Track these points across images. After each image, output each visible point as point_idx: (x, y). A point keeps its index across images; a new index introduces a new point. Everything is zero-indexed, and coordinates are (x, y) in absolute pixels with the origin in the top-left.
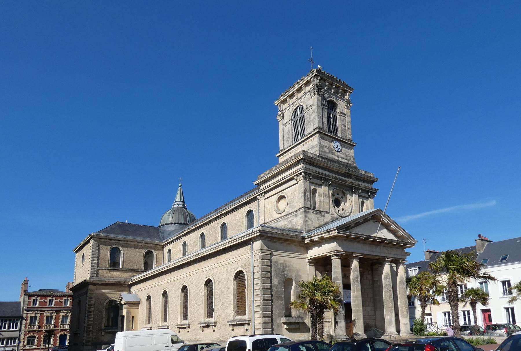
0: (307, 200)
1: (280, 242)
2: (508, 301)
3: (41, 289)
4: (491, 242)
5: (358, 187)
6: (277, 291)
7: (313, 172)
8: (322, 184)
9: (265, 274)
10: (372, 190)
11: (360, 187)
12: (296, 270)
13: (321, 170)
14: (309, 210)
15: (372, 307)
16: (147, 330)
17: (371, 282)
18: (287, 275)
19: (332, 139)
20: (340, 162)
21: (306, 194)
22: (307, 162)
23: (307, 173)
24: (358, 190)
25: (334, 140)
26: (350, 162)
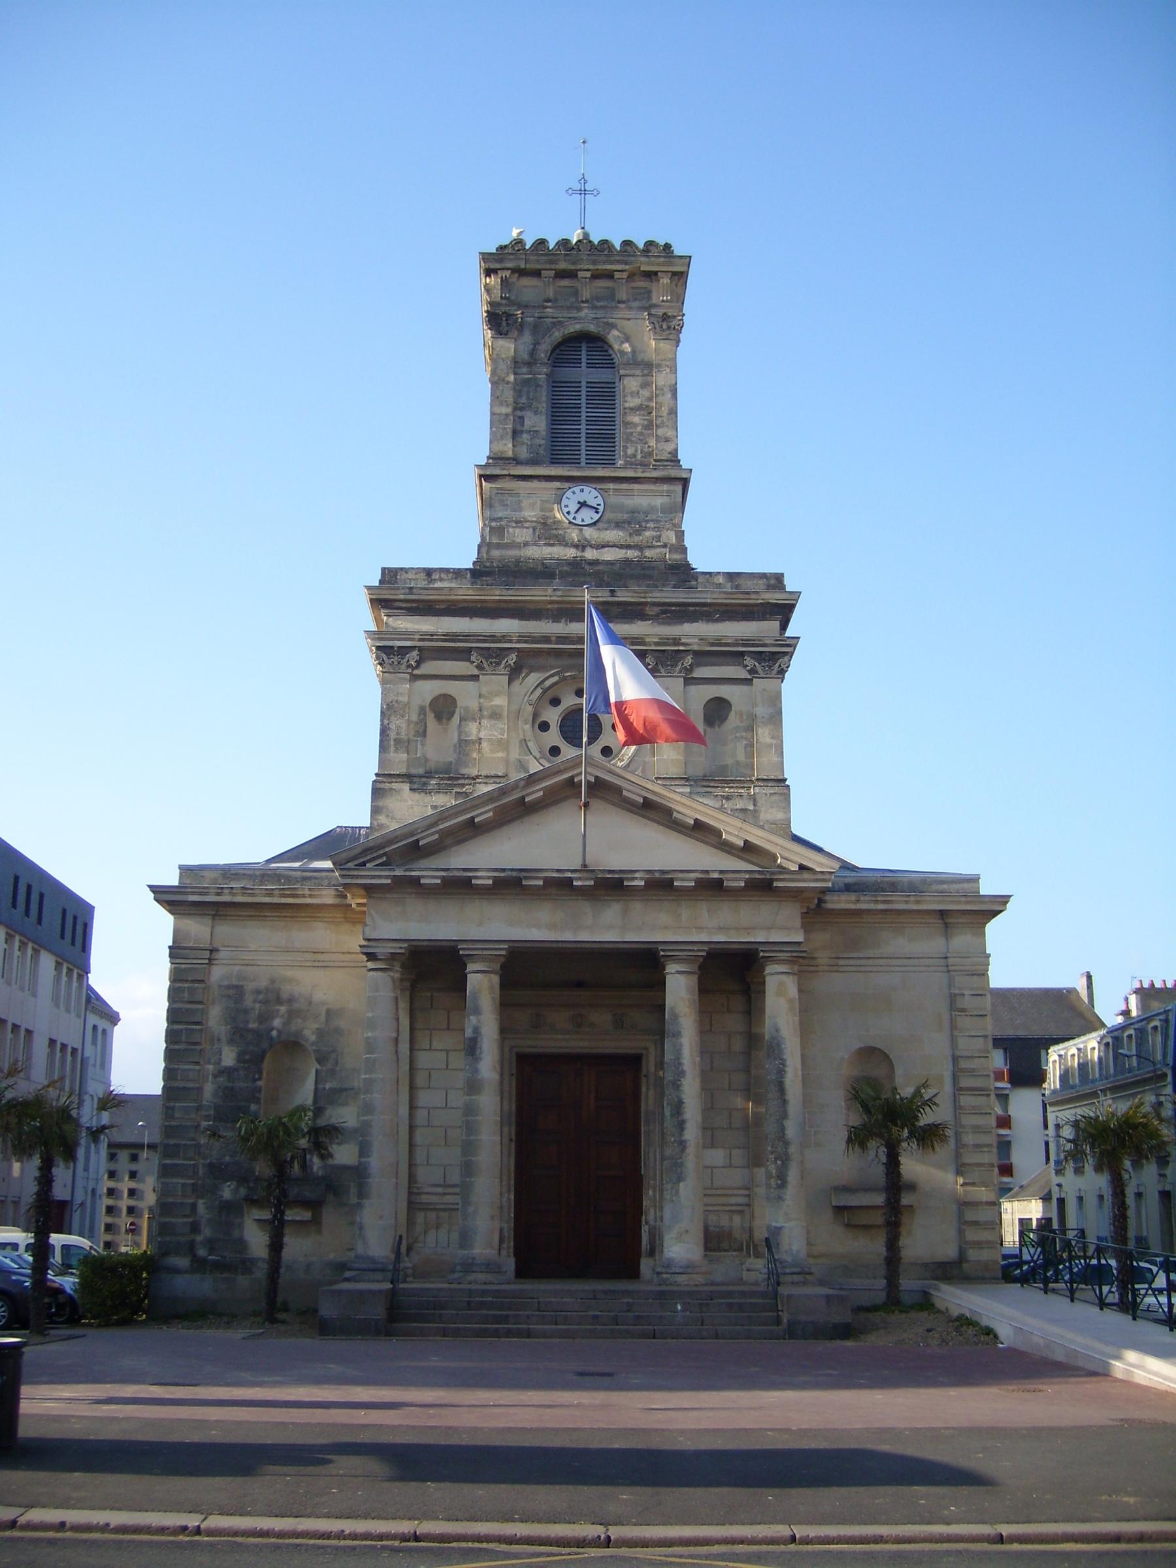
0: (392, 749)
1: (257, 914)
2: (1073, 1174)
3: (1093, 978)
4: (5, 949)
5: (676, 648)
6: (232, 1089)
7: (420, 640)
8: (476, 672)
9: (182, 1030)
10: (758, 645)
11: (681, 648)
12: (324, 1013)
13: (474, 619)
14: (394, 786)
15: (735, 1152)
16: (1047, 1144)
17: (738, 1045)
18: (278, 1030)
19: (558, 484)
20: (587, 567)
21: (393, 726)
22: (401, 608)
23: (392, 647)
24: (678, 661)
25: (566, 485)
26: (648, 553)
